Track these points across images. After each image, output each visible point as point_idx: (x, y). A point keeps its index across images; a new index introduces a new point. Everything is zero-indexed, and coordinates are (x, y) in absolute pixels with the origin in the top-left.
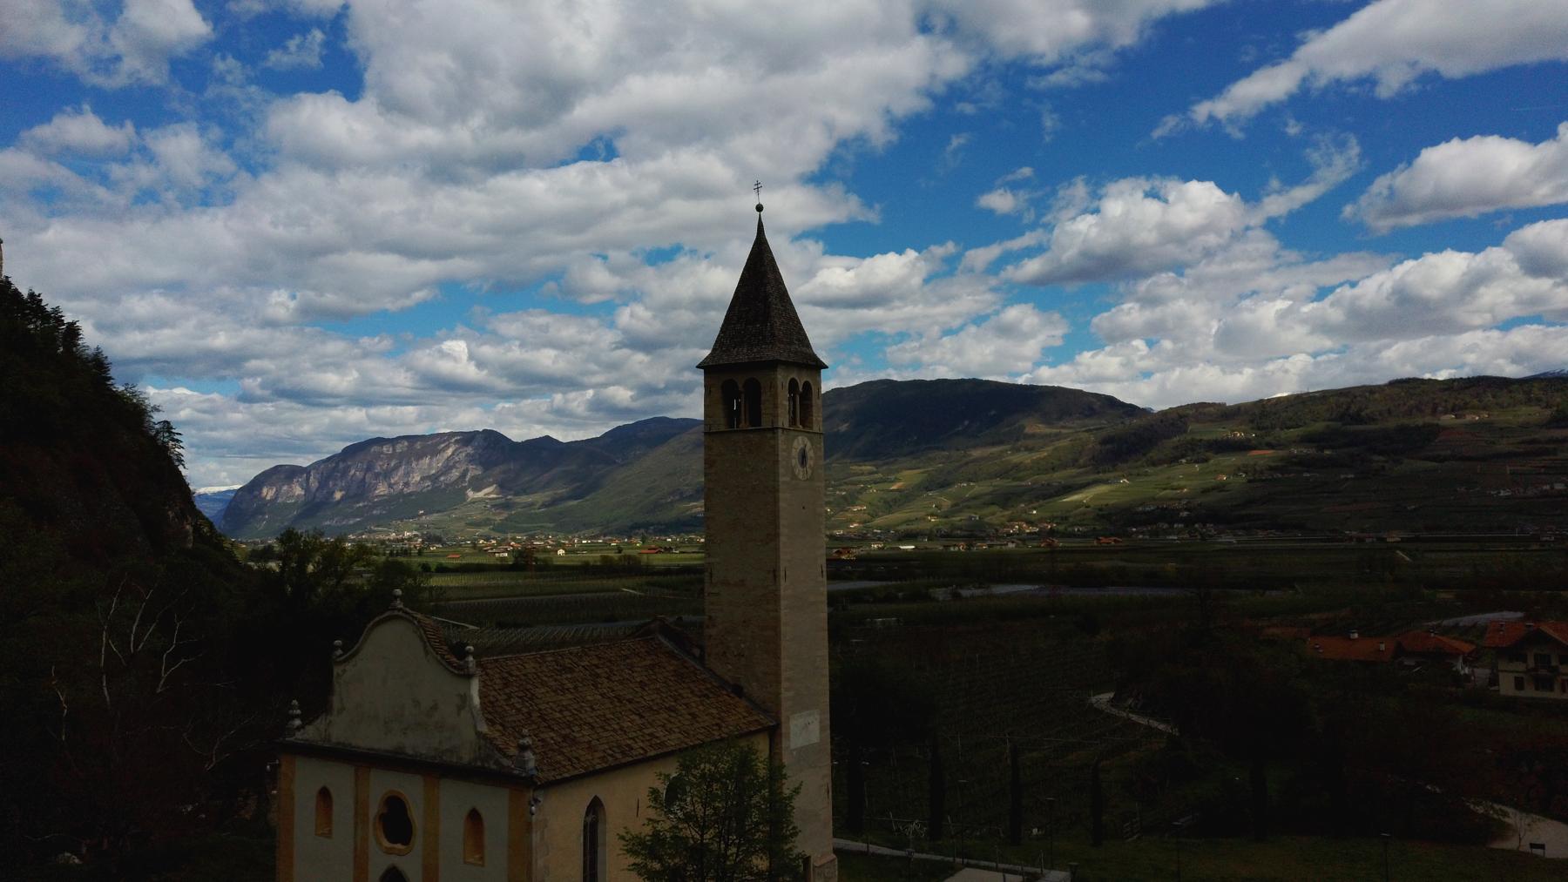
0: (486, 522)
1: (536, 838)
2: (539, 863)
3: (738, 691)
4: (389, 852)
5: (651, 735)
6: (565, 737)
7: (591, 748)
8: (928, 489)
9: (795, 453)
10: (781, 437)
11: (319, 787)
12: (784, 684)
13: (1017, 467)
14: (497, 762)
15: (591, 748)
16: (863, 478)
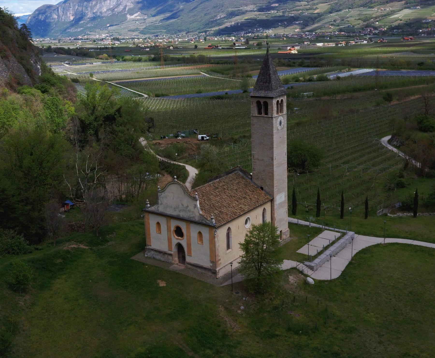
0: (136, 30)
1: (216, 239)
2: (217, 245)
3: (262, 188)
4: (177, 239)
5: (241, 207)
6: (220, 212)
7: (227, 214)
8: (331, 13)
9: (279, 120)
10: (274, 119)
11: (157, 222)
12: (275, 188)
14: (205, 221)
15: (227, 214)
16: (301, 8)
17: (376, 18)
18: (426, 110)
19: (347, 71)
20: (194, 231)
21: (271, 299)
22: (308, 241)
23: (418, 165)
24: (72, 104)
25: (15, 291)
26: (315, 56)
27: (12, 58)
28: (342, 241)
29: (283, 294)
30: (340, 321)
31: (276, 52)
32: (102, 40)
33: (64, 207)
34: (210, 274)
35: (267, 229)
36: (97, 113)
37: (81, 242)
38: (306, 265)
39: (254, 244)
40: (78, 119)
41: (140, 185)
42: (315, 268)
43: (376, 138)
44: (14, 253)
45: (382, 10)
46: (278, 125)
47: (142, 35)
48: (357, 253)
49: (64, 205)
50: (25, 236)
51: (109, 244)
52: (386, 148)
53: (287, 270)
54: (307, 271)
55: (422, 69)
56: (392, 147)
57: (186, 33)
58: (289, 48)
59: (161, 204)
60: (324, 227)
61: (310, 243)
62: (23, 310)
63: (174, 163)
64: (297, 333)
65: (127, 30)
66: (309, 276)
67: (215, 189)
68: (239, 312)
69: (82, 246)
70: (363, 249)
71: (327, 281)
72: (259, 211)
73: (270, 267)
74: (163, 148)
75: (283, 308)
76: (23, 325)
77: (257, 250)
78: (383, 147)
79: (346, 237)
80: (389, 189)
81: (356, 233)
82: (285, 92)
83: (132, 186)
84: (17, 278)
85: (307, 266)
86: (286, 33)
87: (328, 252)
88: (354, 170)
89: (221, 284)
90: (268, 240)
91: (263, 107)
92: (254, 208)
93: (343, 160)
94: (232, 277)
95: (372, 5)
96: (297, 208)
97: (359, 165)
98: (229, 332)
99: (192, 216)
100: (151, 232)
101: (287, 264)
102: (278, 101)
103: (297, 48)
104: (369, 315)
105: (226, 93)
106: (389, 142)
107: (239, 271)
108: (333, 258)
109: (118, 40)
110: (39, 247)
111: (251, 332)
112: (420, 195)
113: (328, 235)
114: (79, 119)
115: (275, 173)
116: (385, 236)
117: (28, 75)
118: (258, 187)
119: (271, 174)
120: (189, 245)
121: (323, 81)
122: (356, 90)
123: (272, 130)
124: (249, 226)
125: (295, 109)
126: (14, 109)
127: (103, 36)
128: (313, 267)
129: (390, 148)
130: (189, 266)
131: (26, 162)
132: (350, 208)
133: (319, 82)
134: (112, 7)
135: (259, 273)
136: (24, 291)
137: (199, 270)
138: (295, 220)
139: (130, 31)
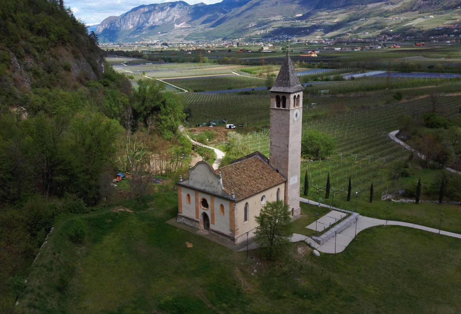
1: (235, 212)
2: (236, 216)
3: (277, 171)
4: (203, 209)
6: (240, 189)
9: (295, 112)
10: (291, 111)
12: (289, 171)
13: (387, 12)
15: (245, 191)
16: (323, 17)
17: (391, 26)
18: (434, 108)
19: (361, 73)
20: (216, 204)
21: (281, 266)
22: (316, 218)
23: (423, 157)
24: (127, 96)
25: (74, 242)
26: (333, 59)
27: (83, 59)
28: (347, 220)
29: (291, 262)
30: (341, 290)
31: (299, 55)
32: (154, 44)
33: (116, 178)
34: (229, 240)
35: (279, 207)
36: (147, 104)
37: (127, 207)
38: (313, 239)
39: (267, 218)
40: (131, 109)
41: (177, 164)
42: (321, 242)
43: (385, 132)
44: (75, 212)
45: (396, 19)
46: (294, 117)
47: (186, 41)
48: (360, 232)
49: (116, 176)
50: (84, 199)
51: (149, 209)
52: (394, 141)
53: (296, 242)
54: (314, 244)
55: (431, 72)
56: (399, 141)
57: (222, 40)
58: (309, 52)
59: (191, 179)
60: (331, 207)
61: (318, 221)
62: (80, 258)
63: (206, 146)
64: (301, 297)
65: (174, 37)
66: (316, 249)
67: (236, 170)
68: (253, 274)
69: (128, 210)
70: (366, 229)
71: (332, 254)
72: (275, 190)
73: (281, 238)
74: (197, 134)
75: (291, 274)
76: (79, 269)
77: (270, 223)
78: (391, 140)
79: (351, 217)
80: (394, 178)
81: (360, 214)
82: (301, 88)
83: (171, 163)
84: (76, 232)
85: (314, 240)
86: (308, 40)
87: (333, 230)
88: (363, 159)
89: (239, 249)
90: (280, 216)
91: (282, 99)
92: (270, 188)
93: (353, 151)
94: (248, 245)
95: (387, 15)
96: (309, 189)
97: (367, 155)
98: (243, 290)
99: (216, 191)
100: (183, 202)
101: (296, 237)
102: (295, 96)
103: (316, 52)
104: (368, 287)
105: (253, 90)
106: (397, 136)
107: (253, 240)
108: (338, 235)
109: (166, 44)
110: (94, 208)
111: (261, 292)
112: (423, 185)
113: (335, 215)
114: (132, 108)
115: (289, 159)
116: (387, 219)
117: (94, 72)
118: (274, 169)
119: (286, 159)
120: (213, 215)
121: (339, 80)
122: (368, 89)
123: (289, 121)
124: (264, 202)
125: (313, 104)
126: (82, 99)
127: (155, 41)
128: (320, 241)
129: (397, 141)
130: (213, 232)
131: (88, 141)
132: (357, 193)
133: (335, 82)
134: (163, 18)
135: (271, 243)
136: (81, 243)
137: (220, 236)
138: (306, 200)
139: (176, 37)
